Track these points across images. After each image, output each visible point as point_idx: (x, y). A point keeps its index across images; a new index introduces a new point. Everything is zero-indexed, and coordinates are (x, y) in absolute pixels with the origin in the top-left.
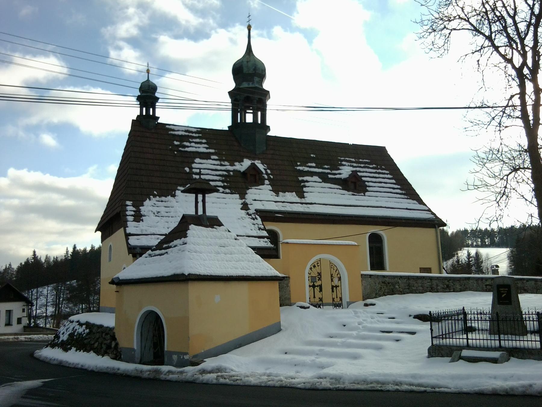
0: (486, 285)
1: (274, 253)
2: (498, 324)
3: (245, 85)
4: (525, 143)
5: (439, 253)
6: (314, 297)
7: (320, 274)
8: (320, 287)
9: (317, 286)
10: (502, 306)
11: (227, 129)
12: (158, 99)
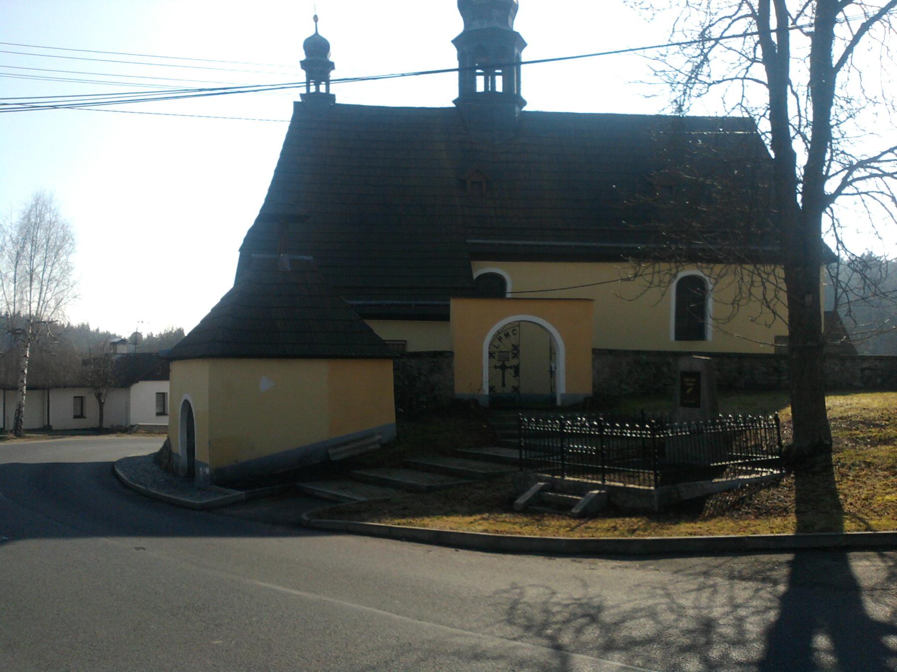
0: (863, 370)
6: (504, 385)
7: (516, 347)
8: (517, 369)
9: (511, 367)
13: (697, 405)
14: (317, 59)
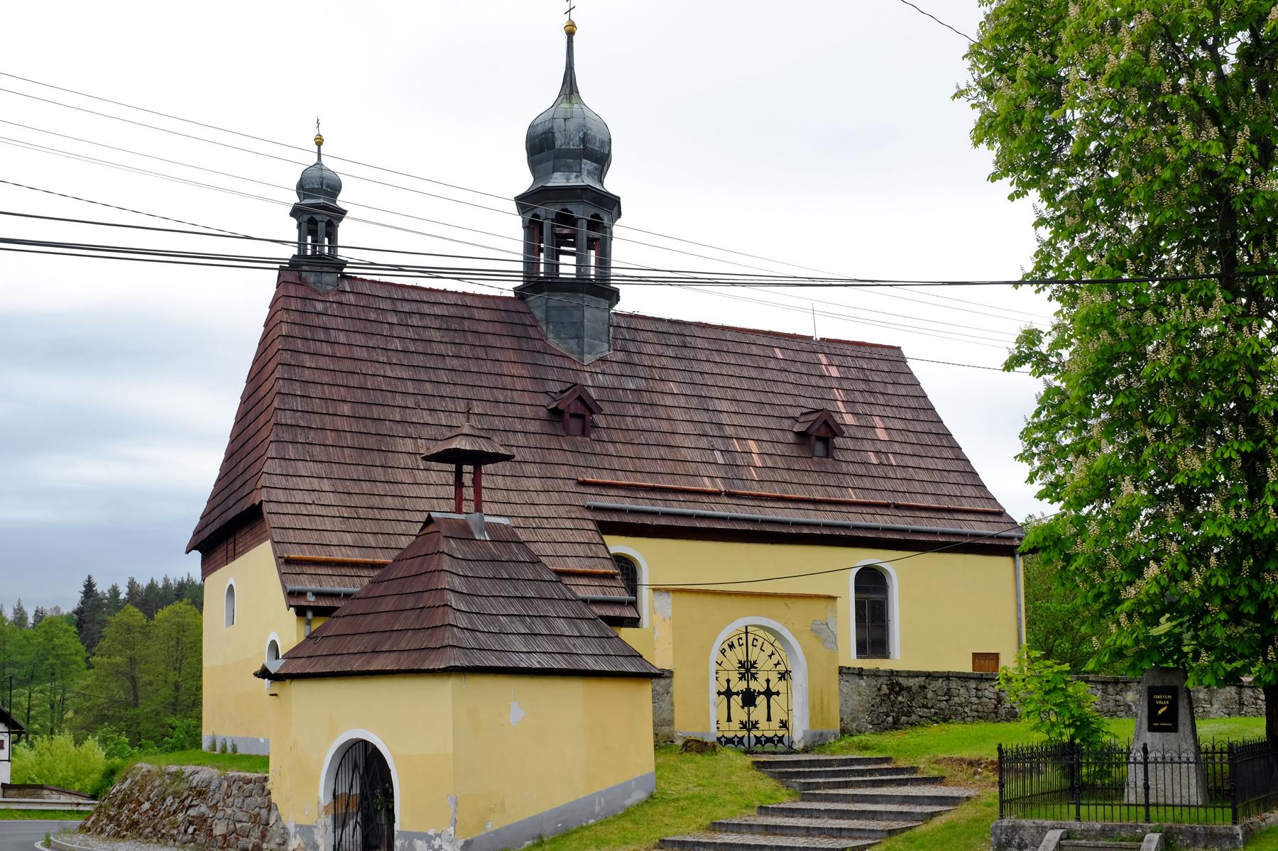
0: (1148, 820)
1: (628, 613)
2: (1147, 795)
3: (558, 180)
4: (1198, 723)
5: (1019, 619)
6: (729, 720)
9: (738, 694)
10: (1158, 735)
11: (512, 294)
12: (344, 212)
13: (1174, 729)
14: (318, 207)
